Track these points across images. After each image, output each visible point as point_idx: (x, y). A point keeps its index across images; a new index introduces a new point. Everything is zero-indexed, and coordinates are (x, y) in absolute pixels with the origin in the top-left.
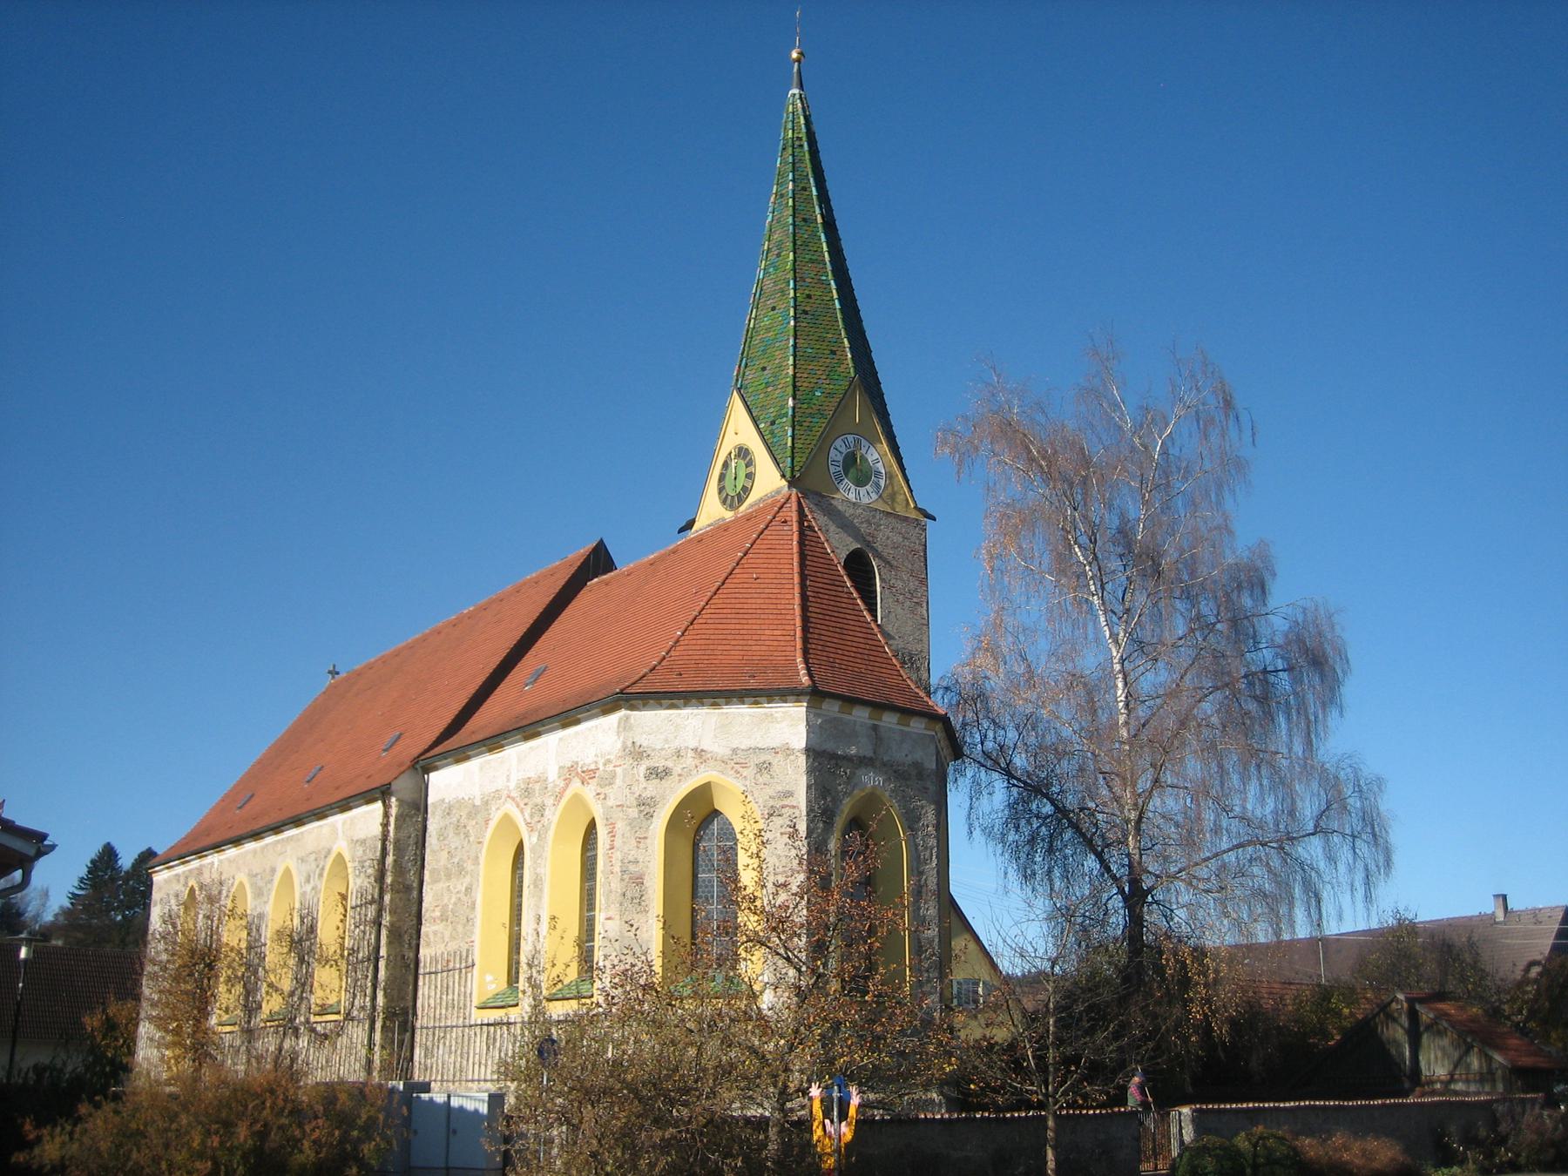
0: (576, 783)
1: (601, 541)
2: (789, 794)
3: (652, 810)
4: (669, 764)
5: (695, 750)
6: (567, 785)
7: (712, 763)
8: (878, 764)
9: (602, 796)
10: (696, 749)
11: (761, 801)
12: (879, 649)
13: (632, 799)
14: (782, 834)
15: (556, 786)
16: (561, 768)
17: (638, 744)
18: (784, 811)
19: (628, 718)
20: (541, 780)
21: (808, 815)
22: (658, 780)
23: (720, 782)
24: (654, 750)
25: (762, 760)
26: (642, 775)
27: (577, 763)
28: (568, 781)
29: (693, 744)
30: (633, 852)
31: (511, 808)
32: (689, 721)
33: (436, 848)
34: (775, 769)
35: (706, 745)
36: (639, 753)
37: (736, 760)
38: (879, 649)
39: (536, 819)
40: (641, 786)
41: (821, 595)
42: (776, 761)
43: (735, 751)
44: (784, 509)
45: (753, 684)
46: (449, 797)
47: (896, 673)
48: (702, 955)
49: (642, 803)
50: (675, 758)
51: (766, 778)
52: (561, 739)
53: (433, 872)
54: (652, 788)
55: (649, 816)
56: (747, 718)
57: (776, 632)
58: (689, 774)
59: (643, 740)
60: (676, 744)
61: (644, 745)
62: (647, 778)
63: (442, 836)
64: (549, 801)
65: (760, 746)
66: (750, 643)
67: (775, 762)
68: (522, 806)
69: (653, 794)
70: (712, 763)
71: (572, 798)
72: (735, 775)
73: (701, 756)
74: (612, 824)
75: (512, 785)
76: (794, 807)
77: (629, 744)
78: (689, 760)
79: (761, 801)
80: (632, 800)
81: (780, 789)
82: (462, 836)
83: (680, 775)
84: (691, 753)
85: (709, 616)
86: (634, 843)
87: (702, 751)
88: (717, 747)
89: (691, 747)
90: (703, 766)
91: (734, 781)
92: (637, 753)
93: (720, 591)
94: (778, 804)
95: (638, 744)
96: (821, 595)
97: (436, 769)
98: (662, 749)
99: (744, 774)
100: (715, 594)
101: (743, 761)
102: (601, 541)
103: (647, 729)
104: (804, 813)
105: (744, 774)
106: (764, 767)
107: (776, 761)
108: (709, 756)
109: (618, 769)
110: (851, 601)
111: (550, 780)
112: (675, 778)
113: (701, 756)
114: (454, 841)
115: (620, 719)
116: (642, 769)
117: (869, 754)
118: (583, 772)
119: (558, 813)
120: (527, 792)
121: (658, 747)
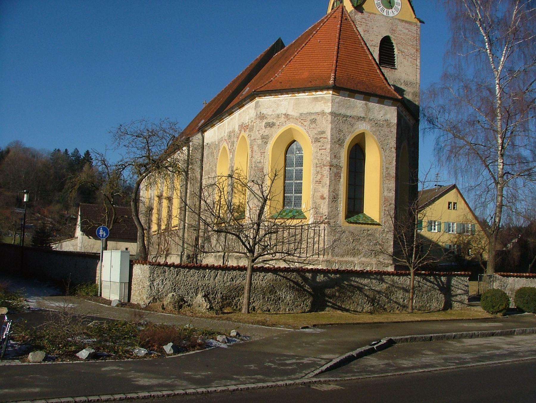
0: (243, 132)
1: (280, 38)
3: (267, 140)
4: (275, 121)
5: (285, 114)
6: (240, 132)
7: (291, 120)
8: (367, 120)
11: (311, 136)
12: (375, 71)
13: (260, 136)
14: (320, 149)
15: (238, 133)
16: (239, 126)
17: (262, 113)
20: (234, 131)
23: (294, 128)
24: (268, 115)
25: (313, 118)
26: (263, 126)
27: (243, 123)
28: (240, 131)
29: (284, 112)
30: (259, 159)
34: (318, 122)
36: (262, 117)
37: (302, 118)
38: (375, 71)
39: (232, 148)
40: (263, 131)
41: (347, 48)
42: (319, 118)
43: (301, 114)
44: (336, 12)
45: (309, 85)
46: (210, 142)
47: (383, 83)
48: (512, 233)
49: (263, 137)
51: (313, 126)
53: (205, 171)
54: (267, 131)
55: (266, 143)
56: (307, 100)
57: (324, 64)
58: (283, 125)
59: (264, 111)
60: (278, 112)
62: (266, 127)
63: (208, 157)
64: (235, 140)
65: (311, 112)
66: (313, 68)
67: (318, 119)
68: (228, 142)
70: (291, 120)
71: (242, 137)
72: (301, 125)
73: (287, 117)
76: (325, 138)
77: (259, 113)
78: (282, 119)
79: (311, 136)
81: (319, 130)
82: (213, 156)
83: (278, 125)
84: (283, 116)
85: (297, 58)
87: (288, 115)
89: (283, 113)
90: (288, 121)
91: (301, 128)
94: (319, 137)
95: (262, 113)
97: (206, 131)
98: (272, 115)
99: (305, 124)
100: (301, 49)
101: (305, 119)
102: (280, 38)
103: (265, 106)
104: (329, 140)
105: (305, 124)
106: (314, 121)
107: (319, 118)
108: (290, 117)
109: (254, 124)
110: (363, 51)
111: (236, 131)
112: (276, 127)
113: (287, 117)
115: (256, 102)
116: (264, 123)
117: (363, 115)
118: (245, 127)
119: (237, 146)
121: (270, 114)
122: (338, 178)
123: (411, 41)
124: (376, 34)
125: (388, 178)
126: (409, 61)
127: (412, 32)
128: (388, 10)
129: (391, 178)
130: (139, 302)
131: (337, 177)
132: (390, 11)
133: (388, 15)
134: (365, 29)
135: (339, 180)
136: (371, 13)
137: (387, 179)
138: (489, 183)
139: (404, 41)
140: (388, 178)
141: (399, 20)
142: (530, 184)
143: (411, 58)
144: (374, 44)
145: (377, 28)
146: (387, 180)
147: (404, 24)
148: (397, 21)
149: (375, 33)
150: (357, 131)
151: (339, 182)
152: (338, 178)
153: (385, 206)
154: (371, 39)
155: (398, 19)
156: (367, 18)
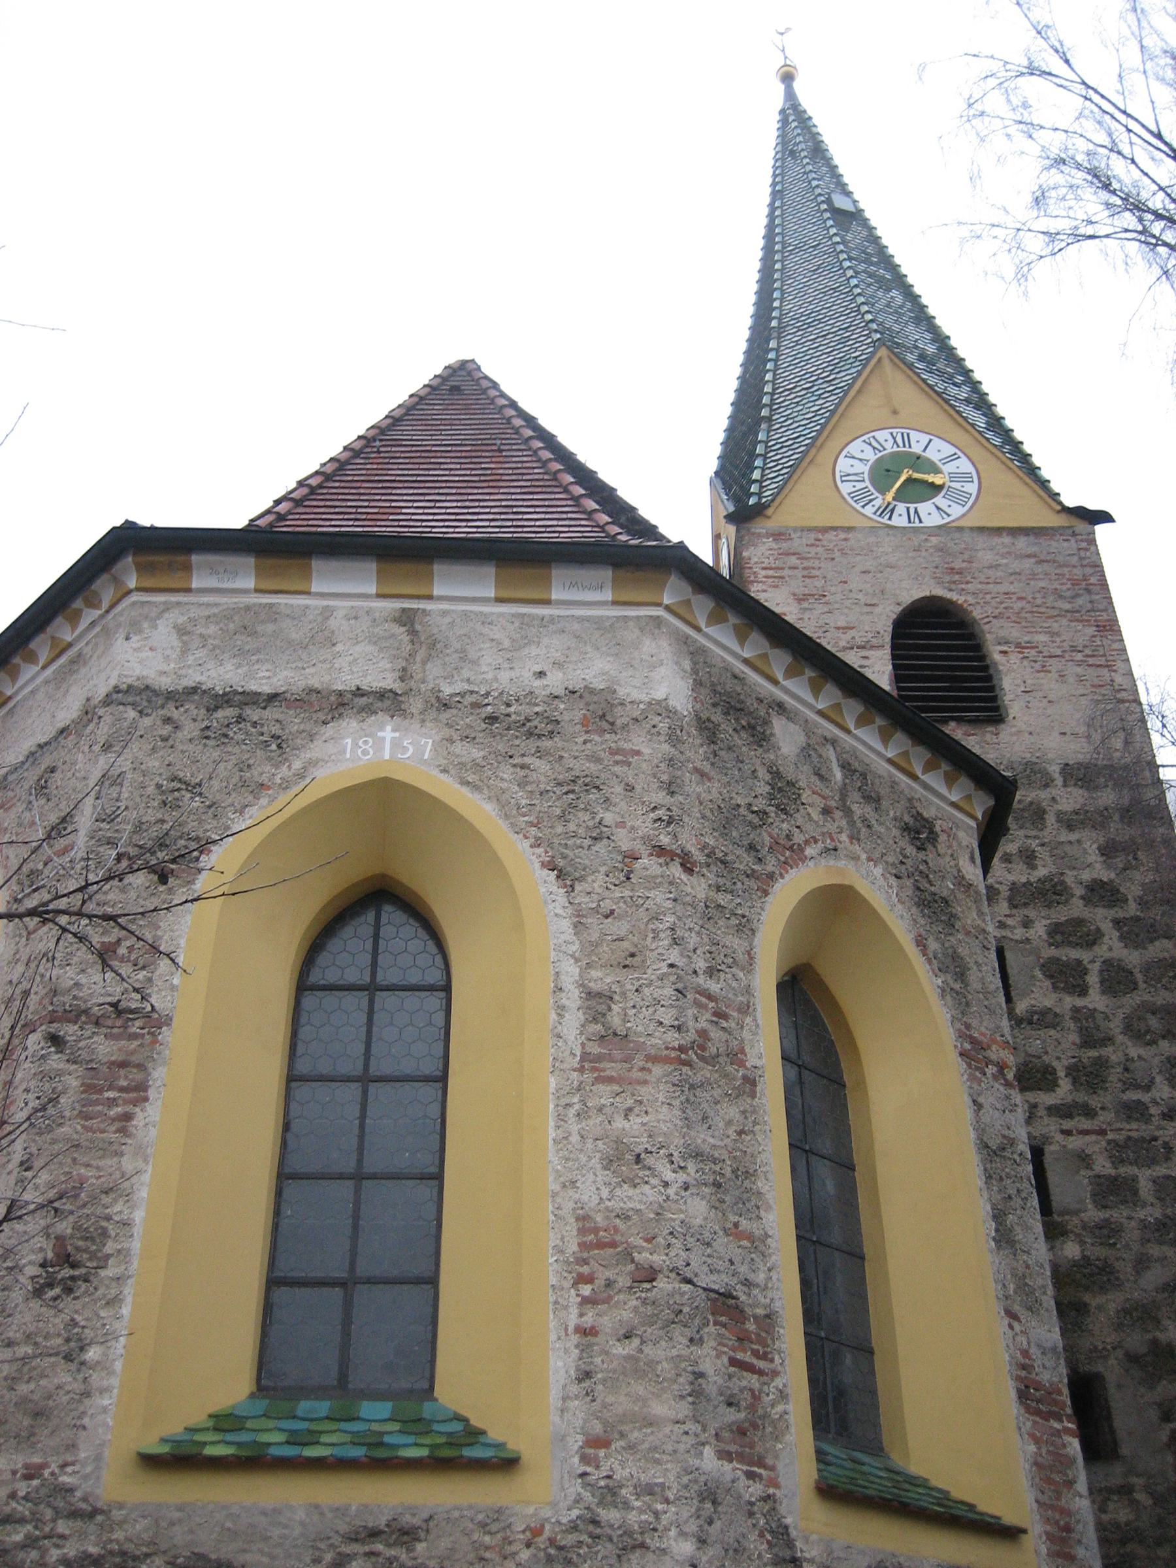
8: (415, 705)
117: (389, 681)
122: (112, 1102)
123: (1061, 597)
124: (863, 599)
125: (611, 1069)
126: (1071, 680)
127: (1054, 562)
128: (912, 506)
129: (639, 1061)
130: (1140, 1178)
131: (111, 1094)
132: (871, 456)
133: (917, 524)
134: (801, 591)
135: (128, 1117)
136: (825, 530)
137: (599, 1080)
138: (767, 1188)
139: (1020, 604)
140: (611, 1069)
141: (981, 530)
142: (1173, 1124)
143: (1079, 664)
144: (859, 641)
145: (868, 577)
146: (600, 1088)
147: (1006, 540)
148: (967, 537)
149: (860, 596)
150: (320, 773)
151: (123, 1131)
152: (112, 1102)
153: (586, 1301)
154: (841, 624)
155: (972, 529)
156: (807, 549)
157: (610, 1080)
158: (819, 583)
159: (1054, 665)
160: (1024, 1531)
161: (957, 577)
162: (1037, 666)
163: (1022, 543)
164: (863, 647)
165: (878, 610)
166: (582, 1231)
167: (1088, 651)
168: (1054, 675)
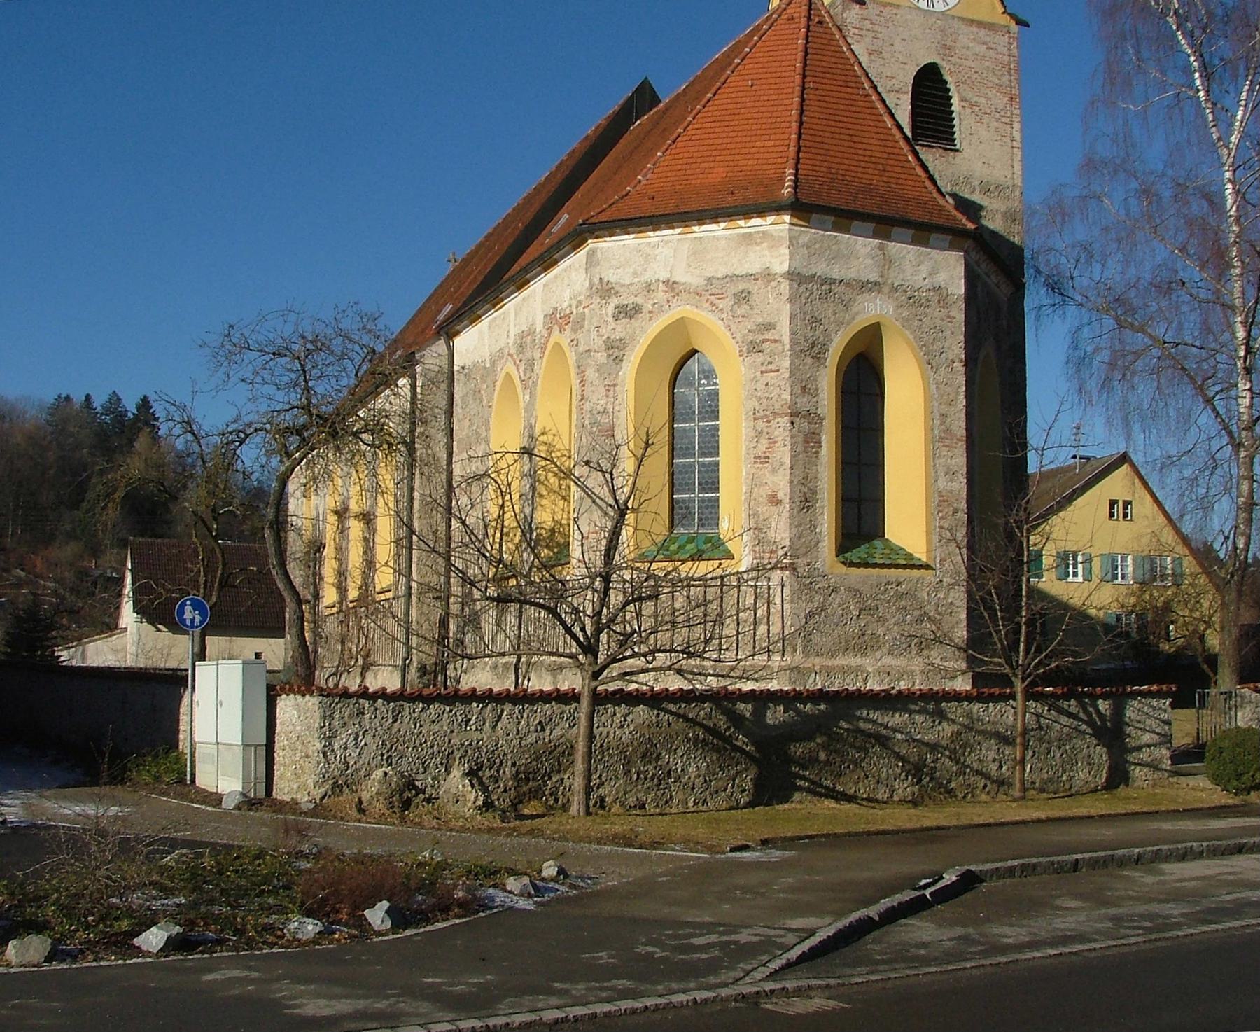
2: (769, 327)
3: (622, 353)
4: (639, 300)
5: (666, 282)
8: (886, 289)
9: (575, 343)
10: (668, 281)
11: (739, 336)
16: (546, 316)
17: (606, 280)
18: (765, 345)
19: (592, 253)
20: (531, 332)
21: (792, 349)
22: (628, 320)
24: (623, 286)
25: (741, 288)
26: (610, 314)
28: (550, 330)
29: (664, 276)
31: (510, 367)
32: (660, 249)
33: (461, 417)
34: (755, 298)
35: (680, 276)
37: (711, 290)
39: (528, 375)
40: (610, 327)
41: (827, 99)
42: (755, 288)
43: (709, 280)
46: (468, 363)
47: (924, 190)
50: (646, 293)
52: (545, 285)
54: (620, 329)
55: (619, 360)
58: (661, 310)
59: (611, 276)
60: (647, 277)
61: (612, 280)
62: (616, 318)
64: (537, 354)
65: (737, 273)
69: (622, 335)
73: (673, 290)
74: (583, 372)
75: (511, 341)
76: (776, 341)
77: (596, 281)
78: (660, 295)
79: (739, 336)
80: (600, 342)
81: (760, 320)
83: (650, 312)
84: (662, 287)
86: (602, 390)
87: (674, 282)
88: (689, 277)
91: (710, 316)
92: (605, 290)
93: (710, 103)
94: (759, 338)
95: (606, 280)
96: (827, 99)
97: (457, 333)
98: (631, 284)
99: (721, 306)
101: (718, 291)
103: (614, 263)
104: (787, 347)
105: (721, 306)
107: (755, 288)
109: (586, 310)
110: (869, 105)
112: (646, 316)
113: (673, 290)
114: (472, 405)
116: (611, 308)
117: (873, 277)
120: (521, 346)
121: (628, 282)
122: (813, 447)
126: (992, 129)
135: (817, 453)
141: (962, 19)
143: (998, 120)
144: (896, 87)
147: (974, 29)
148: (956, 23)
152: (813, 447)
153: (942, 518)
154: (889, 74)
155: (959, 18)
157: (946, 446)
158: (880, 43)
159: (986, 118)
160: (145, 397)
161: (947, 51)
162: (978, 118)
163: (982, 32)
164: (897, 92)
165: (907, 67)
166: (940, 496)
167: (1002, 113)
168: (985, 126)
